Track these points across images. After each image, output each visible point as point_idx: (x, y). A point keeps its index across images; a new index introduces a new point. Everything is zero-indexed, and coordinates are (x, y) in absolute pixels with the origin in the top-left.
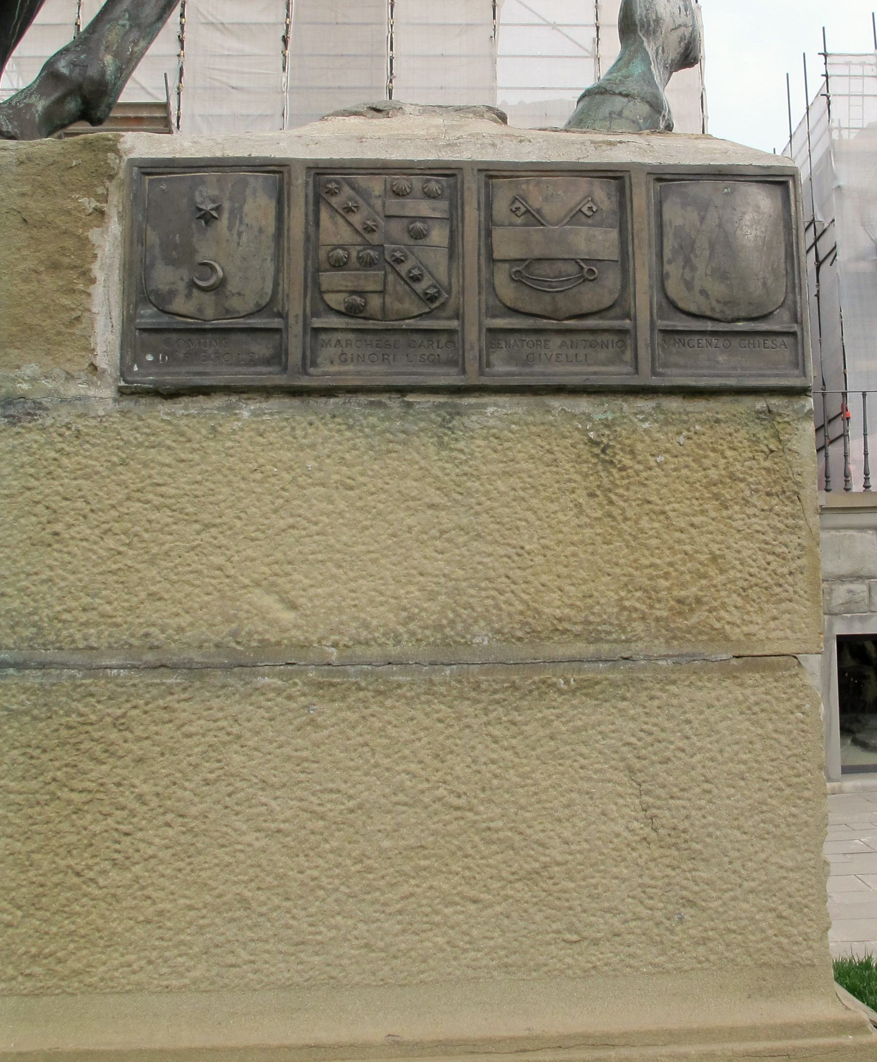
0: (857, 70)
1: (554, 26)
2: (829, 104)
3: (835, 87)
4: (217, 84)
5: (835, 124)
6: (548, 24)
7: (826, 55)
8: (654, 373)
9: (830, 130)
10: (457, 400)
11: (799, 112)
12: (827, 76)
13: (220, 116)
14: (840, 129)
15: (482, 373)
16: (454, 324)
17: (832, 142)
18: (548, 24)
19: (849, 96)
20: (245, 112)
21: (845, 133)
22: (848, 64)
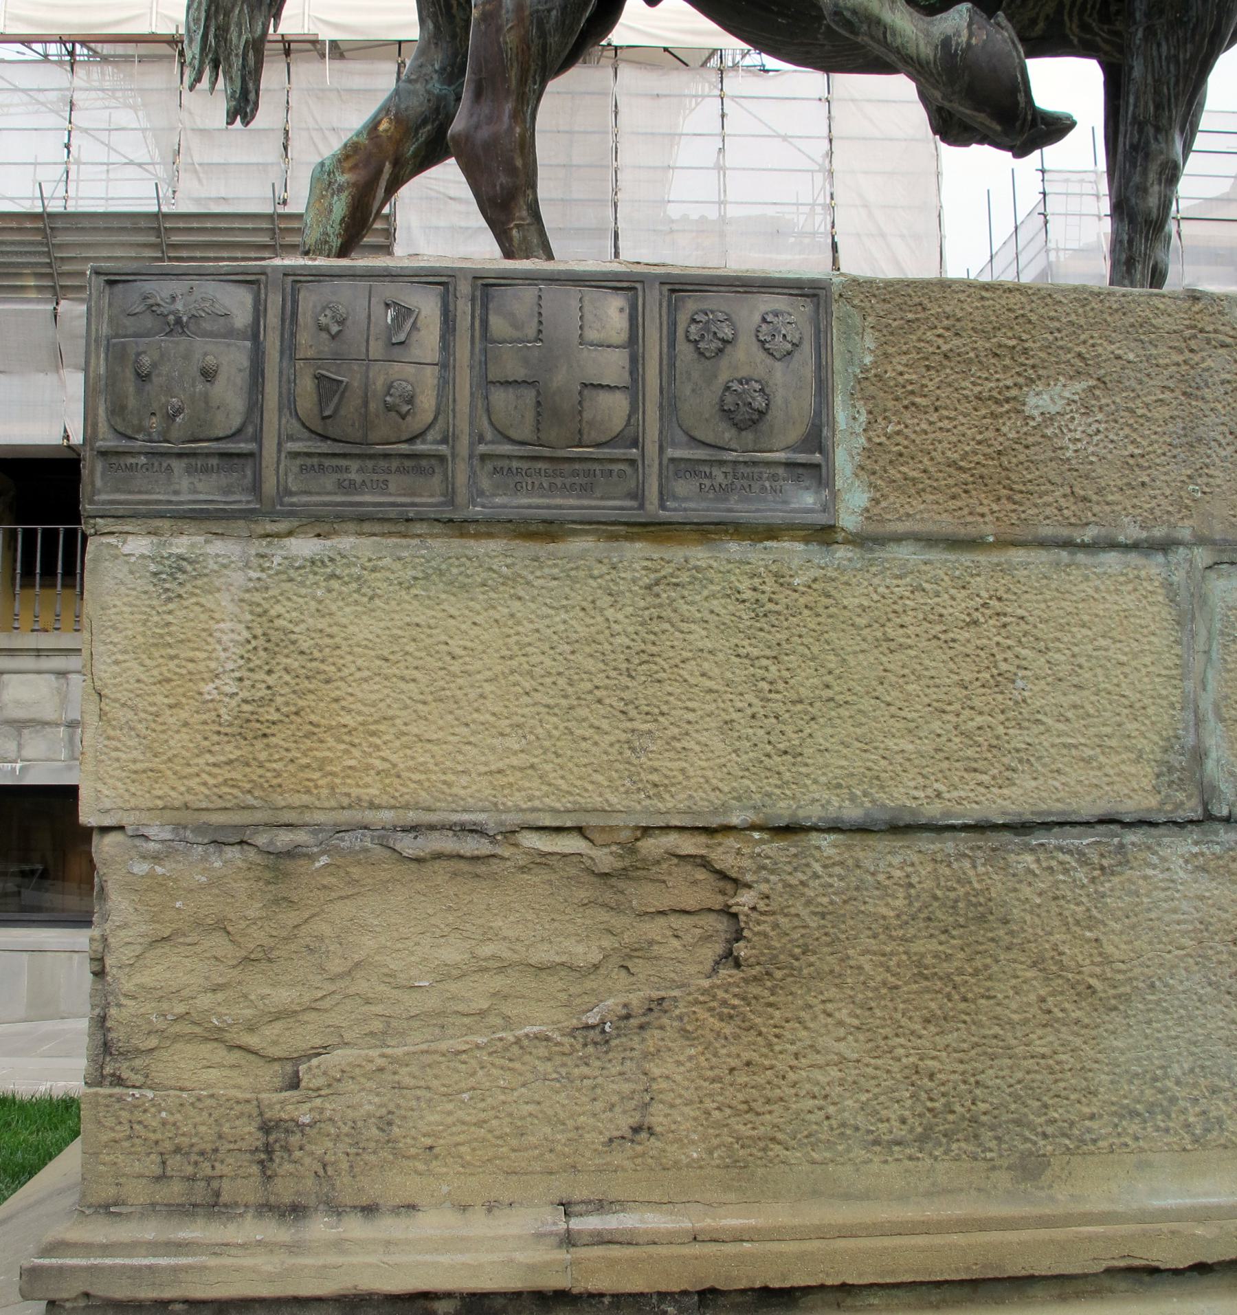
0: (1074, 188)
1: (785, 138)
2: (1046, 222)
3: (1053, 205)
4: (433, 194)
5: (1051, 245)
6: (779, 136)
7: (1043, 171)
8: (663, 507)
9: (1047, 251)
10: (1065, 532)
11: (1003, 230)
12: (1044, 194)
13: (437, 228)
14: (1057, 250)
15: (663, 507)
16: (443, 449)
17: (1049, 264)
18: (779, 136)
19: (35, 164)
20: (463, 224)
21: (1061, 254)
22: (1067, 181)
